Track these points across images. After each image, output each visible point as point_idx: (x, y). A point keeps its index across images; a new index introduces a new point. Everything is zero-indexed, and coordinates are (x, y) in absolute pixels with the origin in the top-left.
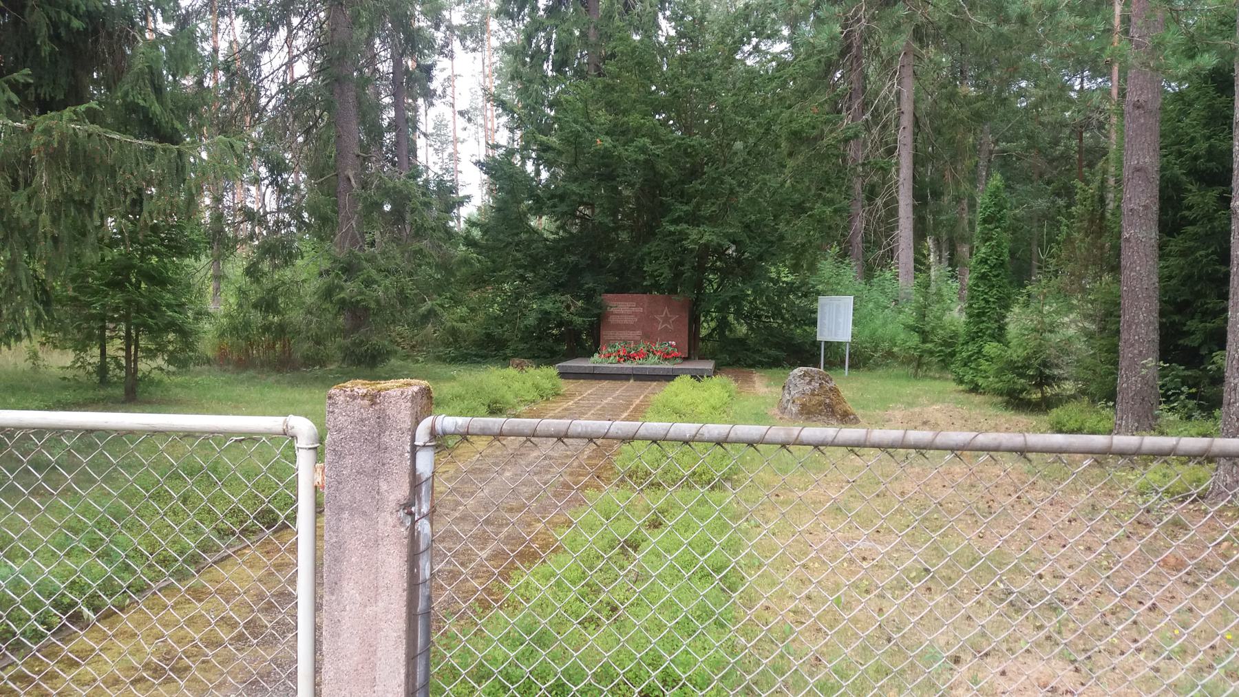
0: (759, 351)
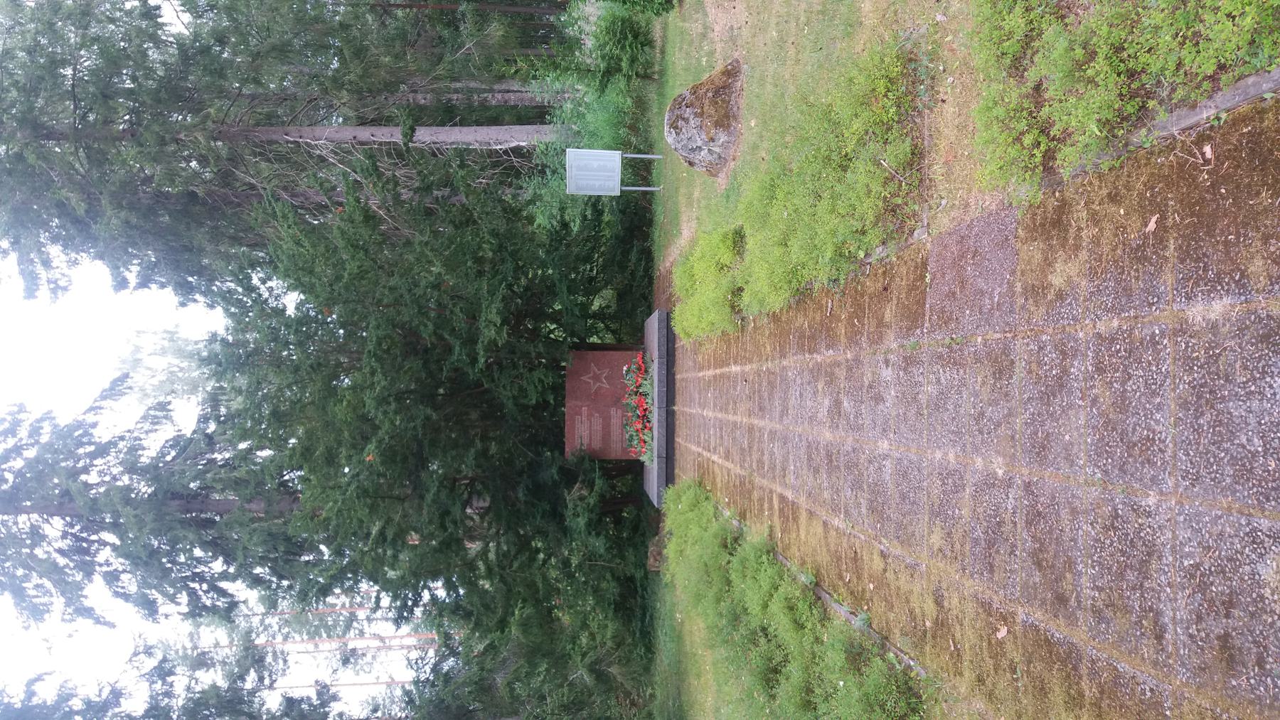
0: (633, 274)
